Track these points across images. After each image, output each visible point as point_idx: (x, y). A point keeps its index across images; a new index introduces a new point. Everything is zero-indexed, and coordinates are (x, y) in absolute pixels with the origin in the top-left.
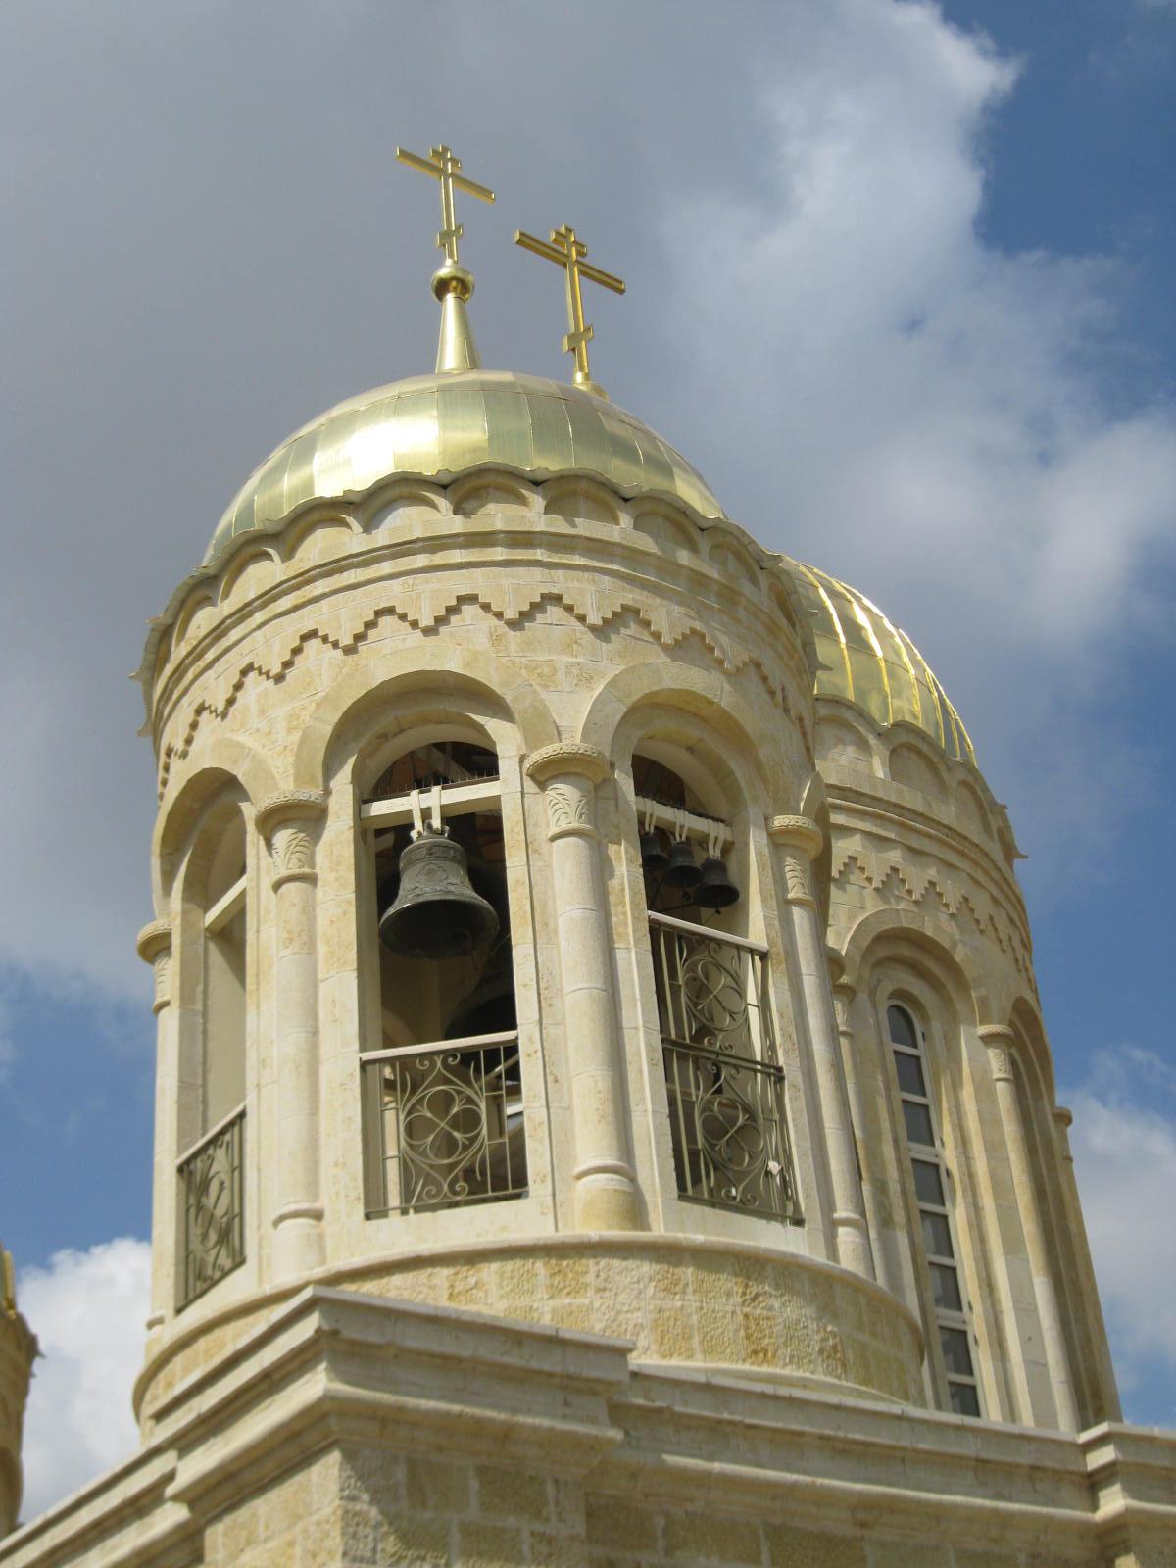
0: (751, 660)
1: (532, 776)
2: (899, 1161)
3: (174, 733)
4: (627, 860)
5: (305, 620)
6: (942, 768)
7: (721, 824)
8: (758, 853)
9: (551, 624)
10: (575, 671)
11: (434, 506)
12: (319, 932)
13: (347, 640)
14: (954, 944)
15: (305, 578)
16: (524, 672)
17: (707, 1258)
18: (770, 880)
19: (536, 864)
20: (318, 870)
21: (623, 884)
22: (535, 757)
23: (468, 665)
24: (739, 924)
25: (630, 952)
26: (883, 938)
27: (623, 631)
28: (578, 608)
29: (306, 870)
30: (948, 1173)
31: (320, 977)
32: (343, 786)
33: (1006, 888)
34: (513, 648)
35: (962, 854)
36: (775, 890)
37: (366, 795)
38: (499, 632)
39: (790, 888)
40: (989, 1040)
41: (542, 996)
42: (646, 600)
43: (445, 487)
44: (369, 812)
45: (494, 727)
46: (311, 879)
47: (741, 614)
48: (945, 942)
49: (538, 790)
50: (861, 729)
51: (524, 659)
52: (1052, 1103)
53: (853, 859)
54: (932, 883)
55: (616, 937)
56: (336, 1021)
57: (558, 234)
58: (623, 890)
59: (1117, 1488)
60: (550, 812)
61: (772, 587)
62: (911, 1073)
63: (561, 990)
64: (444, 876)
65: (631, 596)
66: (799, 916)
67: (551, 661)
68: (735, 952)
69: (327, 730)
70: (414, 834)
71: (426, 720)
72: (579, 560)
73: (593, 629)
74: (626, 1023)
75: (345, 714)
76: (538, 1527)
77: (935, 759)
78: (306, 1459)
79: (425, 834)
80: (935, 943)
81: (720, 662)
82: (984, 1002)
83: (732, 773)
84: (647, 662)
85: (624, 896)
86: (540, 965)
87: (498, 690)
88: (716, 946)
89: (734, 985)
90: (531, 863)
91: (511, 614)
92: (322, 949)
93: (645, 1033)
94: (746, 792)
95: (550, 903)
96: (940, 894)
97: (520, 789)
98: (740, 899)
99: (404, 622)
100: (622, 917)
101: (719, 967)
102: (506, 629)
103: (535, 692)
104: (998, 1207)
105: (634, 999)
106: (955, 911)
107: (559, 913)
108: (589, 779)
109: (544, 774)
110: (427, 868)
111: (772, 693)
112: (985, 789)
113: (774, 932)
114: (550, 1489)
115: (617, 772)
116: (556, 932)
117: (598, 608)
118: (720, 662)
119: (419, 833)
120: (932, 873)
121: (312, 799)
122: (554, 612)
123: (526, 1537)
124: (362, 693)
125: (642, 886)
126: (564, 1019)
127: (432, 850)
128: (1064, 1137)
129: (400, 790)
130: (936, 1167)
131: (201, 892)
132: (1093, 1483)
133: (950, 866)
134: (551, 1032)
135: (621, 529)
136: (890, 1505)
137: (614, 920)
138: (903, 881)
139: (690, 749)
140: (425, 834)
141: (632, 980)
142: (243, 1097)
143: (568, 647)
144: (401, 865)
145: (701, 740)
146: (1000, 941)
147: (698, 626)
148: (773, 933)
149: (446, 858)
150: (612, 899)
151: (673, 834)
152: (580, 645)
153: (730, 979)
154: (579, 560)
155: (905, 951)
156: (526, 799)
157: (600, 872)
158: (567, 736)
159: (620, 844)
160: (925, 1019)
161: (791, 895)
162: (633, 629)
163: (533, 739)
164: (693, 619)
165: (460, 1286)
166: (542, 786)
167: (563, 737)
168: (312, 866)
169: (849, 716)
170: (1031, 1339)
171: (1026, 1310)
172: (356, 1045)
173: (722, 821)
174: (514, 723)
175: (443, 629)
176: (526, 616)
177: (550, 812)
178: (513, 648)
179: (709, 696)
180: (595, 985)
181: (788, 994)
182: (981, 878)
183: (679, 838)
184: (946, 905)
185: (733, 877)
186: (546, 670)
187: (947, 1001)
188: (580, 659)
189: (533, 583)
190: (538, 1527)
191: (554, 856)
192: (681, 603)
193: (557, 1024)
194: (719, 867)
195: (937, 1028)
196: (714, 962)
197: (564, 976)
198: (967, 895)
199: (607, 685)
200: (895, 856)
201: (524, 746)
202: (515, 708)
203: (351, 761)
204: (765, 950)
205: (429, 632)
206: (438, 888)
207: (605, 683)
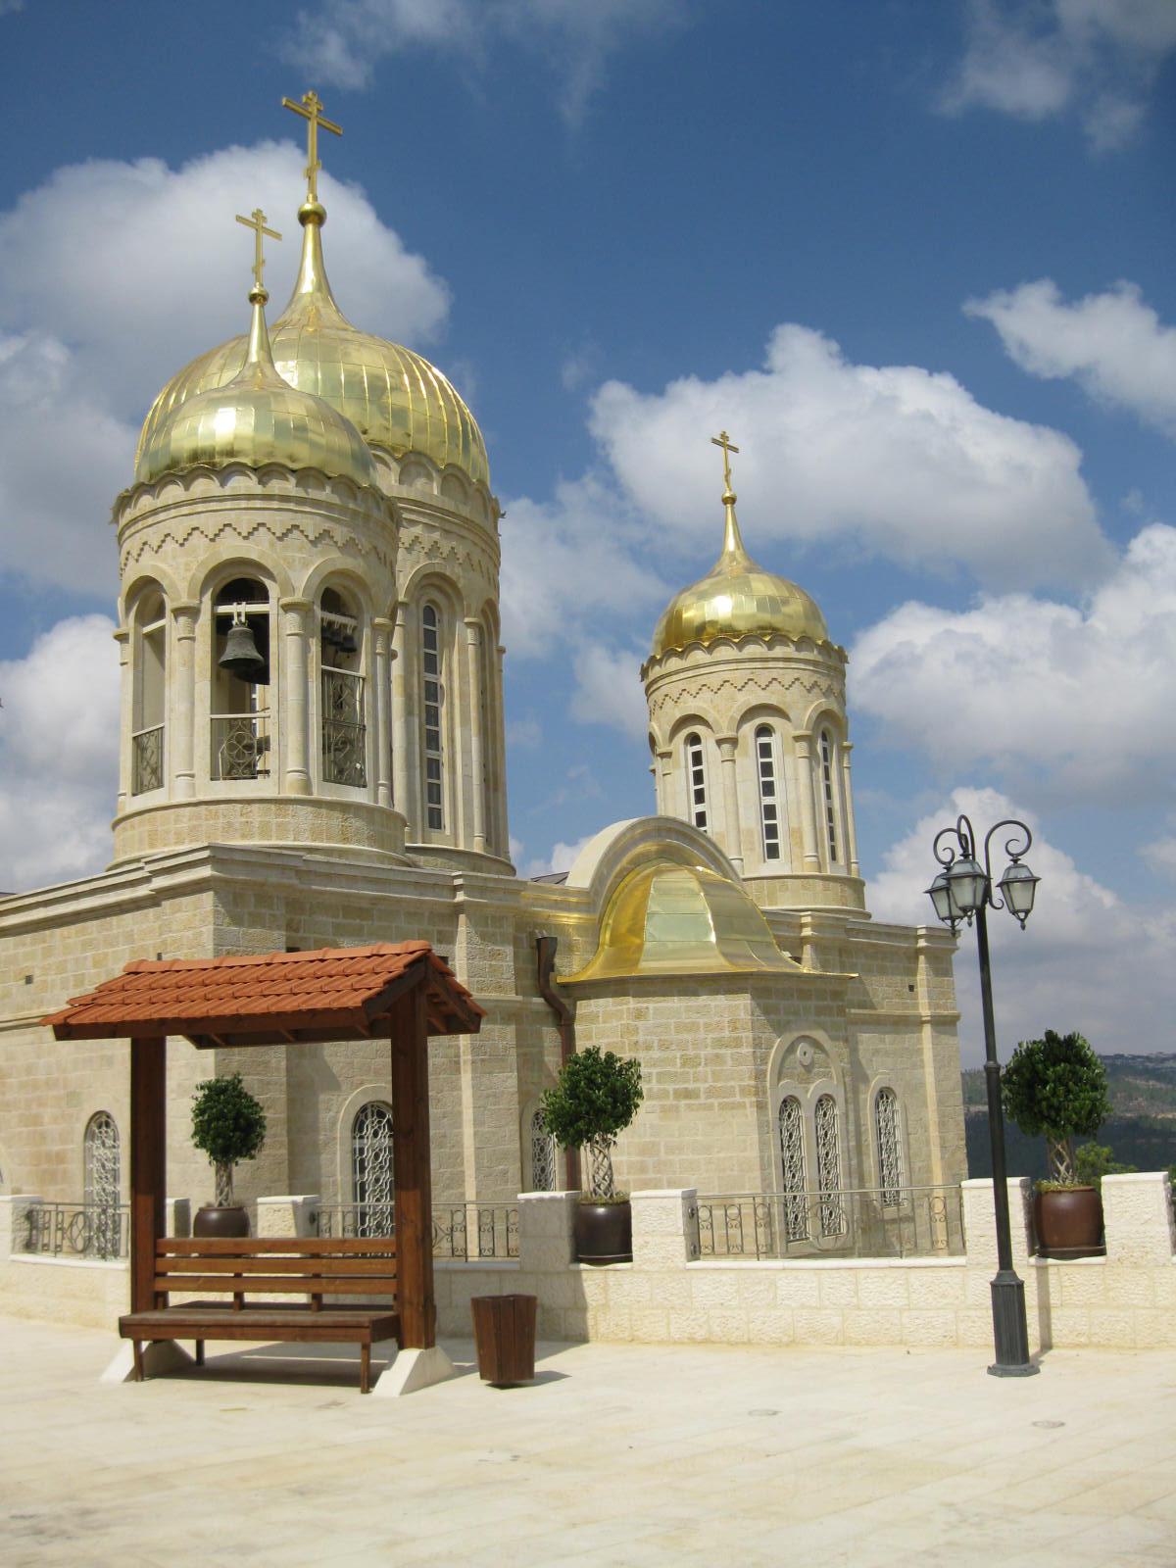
2: (419, 683)
3: (132, 544)
5: (194, 521)
6: (466, 485)
8: (367, 635)
10: (302, 561)
11: (250, 477)
14: (459, 578)
15: (193, 502)
17: (332, 806)
24: (355, 666)
26: (426, 576)
29: (191, 635)
30: (441, 687)
31: (196, 680)
40: (469, 625)
43: (255, 470)
45: (268, 583)
46: (192, 639)
48: (454, 578)
50: (430, 468)
52: (497, 642)
53: (417, 537)
54: (453, 548)
59: (462, 892)
62: (430, 639)
65: (327, 525)
66: (379, 660)
69: (202, 576)
70: (234, 623)
72: (308, 509)
73: (311, 541)
76: (272, 912)
78: (201, 891)
80: (451, 579)
81: (360, 550)
82: (469, 606)
87: (271, 570)
91: (278, 534)
92: (197, 669)
96: (456, 554)
101: (346, 685)
104: (461, 705)
109: (287, 608)
111: (380, 559)
114: (275, 900)
118: (360, 550)
122: (296, 533)
128: (500, 659)
130: (436, 684)
131: (142, 619)
132: (456, 888)
135: (326, 494)
136: (384, 898)
138: (439, 548)
139: (344, 587)
142: (163, 721)
143: (300, 550)
147: (352, 535)
150: (309, 661)
154: (308, 509)
155: (436, 581)
157: (305, 650)
162: (327, 541)
163: (284, 592)
165: (244, 811)
166: (286, 612)
168: (193, 632)
169: (424, 461)
170: (466, 765)
171: (466, 752)
172: (209, 712)
176: (285, 535)
187: (452, 606)
189: (288, 519)
190: (272, 912)
195: (445, 618)
200: (436, 535)
202: (277, 578)
205: (245, 538)
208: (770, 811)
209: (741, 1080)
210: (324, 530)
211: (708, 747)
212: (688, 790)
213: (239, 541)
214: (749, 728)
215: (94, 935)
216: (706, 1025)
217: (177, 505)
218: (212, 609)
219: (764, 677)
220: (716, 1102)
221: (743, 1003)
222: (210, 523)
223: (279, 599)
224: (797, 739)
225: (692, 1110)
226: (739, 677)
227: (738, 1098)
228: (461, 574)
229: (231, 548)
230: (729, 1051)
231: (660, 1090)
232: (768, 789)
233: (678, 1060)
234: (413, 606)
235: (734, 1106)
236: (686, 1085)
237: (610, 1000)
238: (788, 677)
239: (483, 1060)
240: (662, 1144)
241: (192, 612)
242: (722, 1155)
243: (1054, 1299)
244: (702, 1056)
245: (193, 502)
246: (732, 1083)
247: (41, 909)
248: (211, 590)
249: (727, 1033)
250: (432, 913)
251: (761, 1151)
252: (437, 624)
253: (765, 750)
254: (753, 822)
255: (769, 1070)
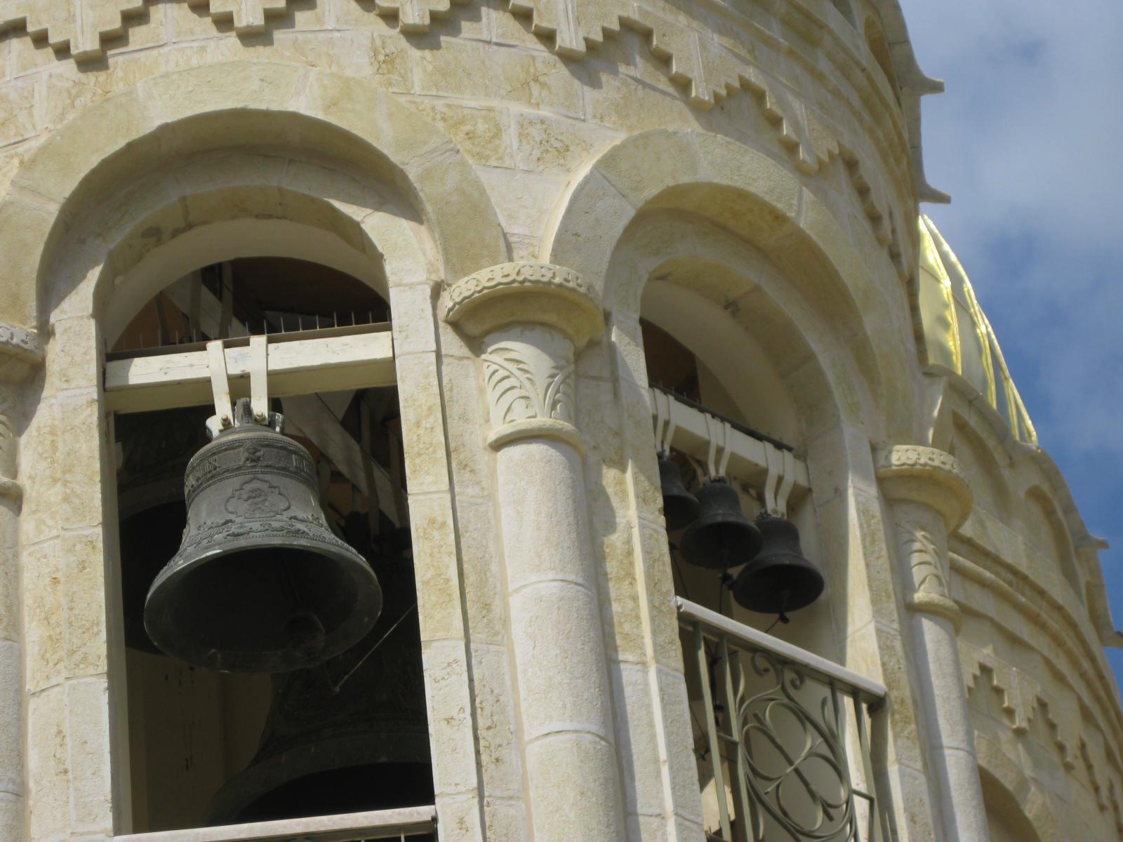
0: (841, 153)
1: (455, 325)
4: (637, 496)
7: (786, 453)
8: (863, 512)
9: (489, 43)
12: (28, 600)
13: (86, 43)
16: (440, 125)
18: (884, 562)
19: (466, 493)
20: (23, 480)
21: (629, 541)
22: (465, 288)
23: (332, 104)
25: (645, 672)
27: (623, 69)
28: (540, 15)
31: (30, 686)
33: (1102, 693)
34: (417, 80)
35: (1034, 619)
38: (390, 48)
39: (917, 584)
41: (482, 743)
42: (661, 14)
44: (127, 377)
47: (824, 66)
49: (465, 351)
51: (439, 104)
54: (986, 670)
55: (619, 642)
56: (66, 771)
58: (630, 553)
60: (491, 396)
61: (869, 25)
63: (518, 732)
64: (283, 506)
67: (490, 110)
68: (827, 692)
70: (214, 424)
71: (239, 208)
73: (568, 58)
74: (642, 807)
75: (87, 181)
77: (991, 443)
79: (237, 424)
83: (810, 357)
84: (671, 129)
85: (632, 564)
86: (476, 683)
87: (395, 158)
88: (794, 676)
89: (829, 754)
90: (457, 489)
93: (679, 826)
94: (837, 394)
95: (494, 567)
96: (999, 691)
97: (434, 348)
98: (823, 596)
99: (200, 15)
100: (630, 604)
102: (403, 42)
103: (463, 163)
105: (656, 761)
106: (1024, 725)
107: (511, 587)
108: (566, 336)
110: (249, 487)
112: (1069, 509)
113: (894, 660)
115: (614, 329)
116: (506, 622)
117: (578, 21)
119: (226, 424)
120: (986, 654)
121: (15, 341)
124: (121, 143)
125: (665, 548)
126: (525, 787)
127: (257, 455)
129: (193, 339)
133: (1015, 641)
134: (501, 811)
137: (616, 607)
139: (732, 307)
140: (237, 424)
141: (651, 725)
143: (524, 87)
144: (190, 481)
145: (757, 289)
146: (1097, 789)
147: (752, 74)
148: (892, 664)
149: (284, 471)
150: (612, 567)
151: (703, 465)
152: (543, 85)
153: (820, 740)
156: (444, 368)
158: (522, 253)
159: (624, 470)
161: (919, 596)
162: (640, 68)
164: (747, 63)
166: (476, 344)
167: (515, 255)
173: (790, 449)
174: (420, 222)
175: (280, 35)
177: (491, 396)
178: (417, 80)
179: (780, 206)
180: (587, 726)
181: (922, 780)
182: (1062, 664)
183: (716, 470)
184: (1010, 712)
185: (810, 550)
186: (481, 127)
188: (545, 112)
191: (501, 479)
192: (721, 31)
193: (511, 798)
194: (786, 531)
196: (792, 705)
197: (524, 707)
198: (1046, 700)
199: (599, 162)
201: (441, 266)
202: (426, 192)
203: (94, 275)
204: (881, 693)
205: (251, 37)
206: (276, 524)
207: (594, 161)
210: (626, 24)
218: (103, 376)
223: (437, 290)
228: (1029, 772)
248: (94, 275)
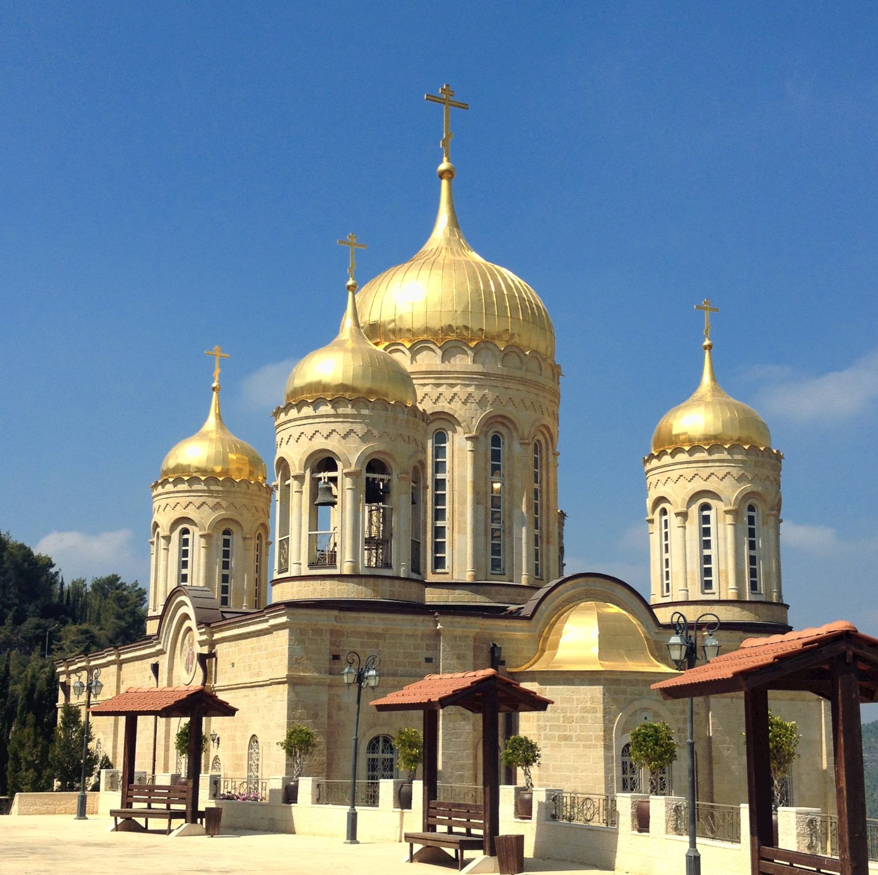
32: (308, 472)
36: (124, 773)
37: (312, 472)
57: (442, 89)
109: (347, 475)
111: (404, 440)
123: (319, 640)
143: (354, 443)
155: (499, 420)
160: (504, 439)
178: (343, 442)
189: (348, 427)
195: (506, 441)
208: (707, 559)
209: (596, 732)
211: (671, 517)
212: (661, 544)
213: (323, 440)
214: (695, 509)
215: (255, 645)
216: (578, 699)
217: (295, 420)
219: (705, 473)
220: (581, 743)
221: (597, 691)
222: (309, 430)
224: (727, 512)
225: (568, 747)
226: (689, 472)
227: (593, 742)
229: (319, 443)
230: (590, 715)
231: (550, 735)
232: (707, 545)
233: (561, 719)
234: (482, 438)
235: (589, 747)
236: (565, 733)
237: (529, 683)
238: (722, 472)
239: (450, 714)
240: (551, 765)
241: (300, 478)
242: (583, 774)
243: (399, 828)
244: (575, 717)
245: (301, 419)
246: (591, 733)
247: (177, 645)
249: (588, 704)
250: (422, 635)
251: (606, 773)
252: (501, 446)
253: (706, 519)
254: (695, 566)
255: (615, 727)
